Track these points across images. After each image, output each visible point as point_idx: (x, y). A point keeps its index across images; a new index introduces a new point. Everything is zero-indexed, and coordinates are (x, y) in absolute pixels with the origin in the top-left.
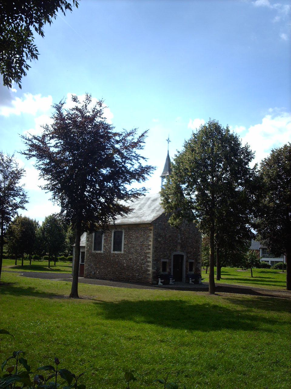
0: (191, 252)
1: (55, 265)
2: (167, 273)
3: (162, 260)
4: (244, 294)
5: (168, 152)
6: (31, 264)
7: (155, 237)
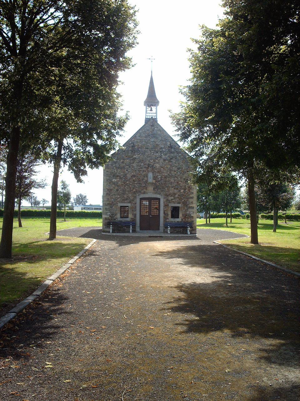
0: (175, 194)
1: (231, 222)
2: (128, 219)
3: (120, 205)
4: (267, 245)
5: (152, 72)
6: (211, 222)
7: (108, 178)
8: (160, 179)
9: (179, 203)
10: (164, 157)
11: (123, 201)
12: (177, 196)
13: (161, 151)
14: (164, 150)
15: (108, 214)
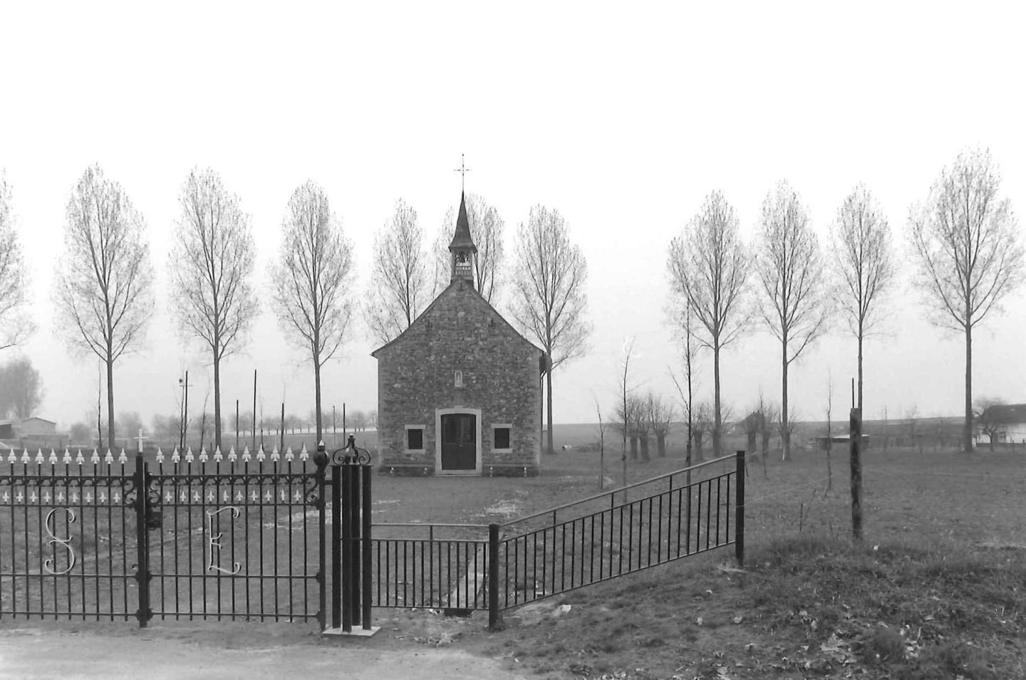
8: (474, 382)
9: (508, 422)
10: (481, 343)
11: (412, 421)
12: (504, 410)
13: (476, 334)
14: (481, 331)
15: (388, 443)
